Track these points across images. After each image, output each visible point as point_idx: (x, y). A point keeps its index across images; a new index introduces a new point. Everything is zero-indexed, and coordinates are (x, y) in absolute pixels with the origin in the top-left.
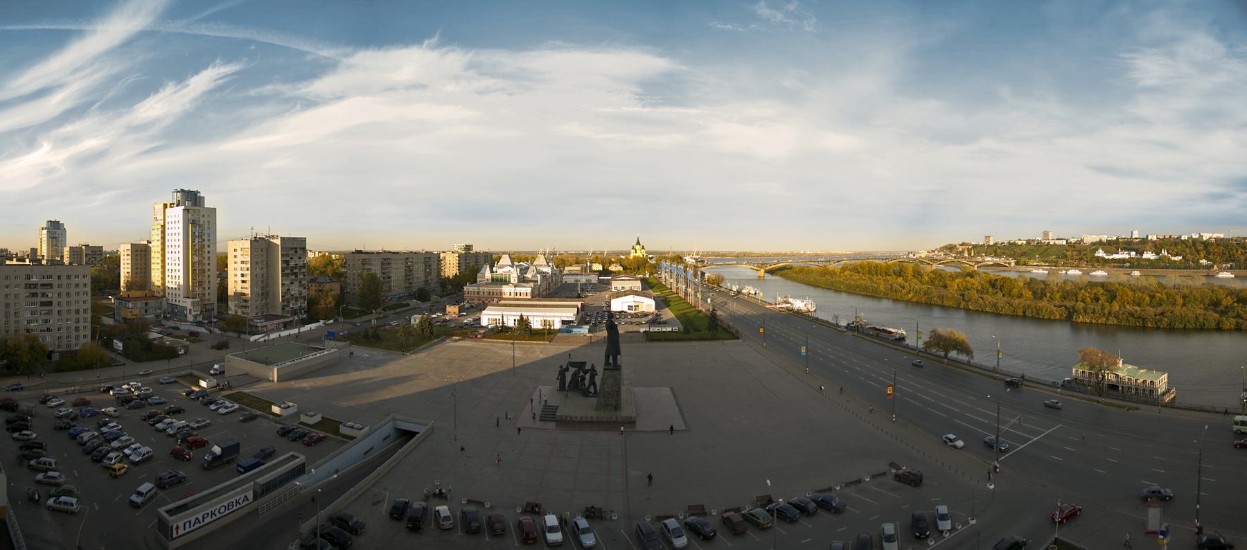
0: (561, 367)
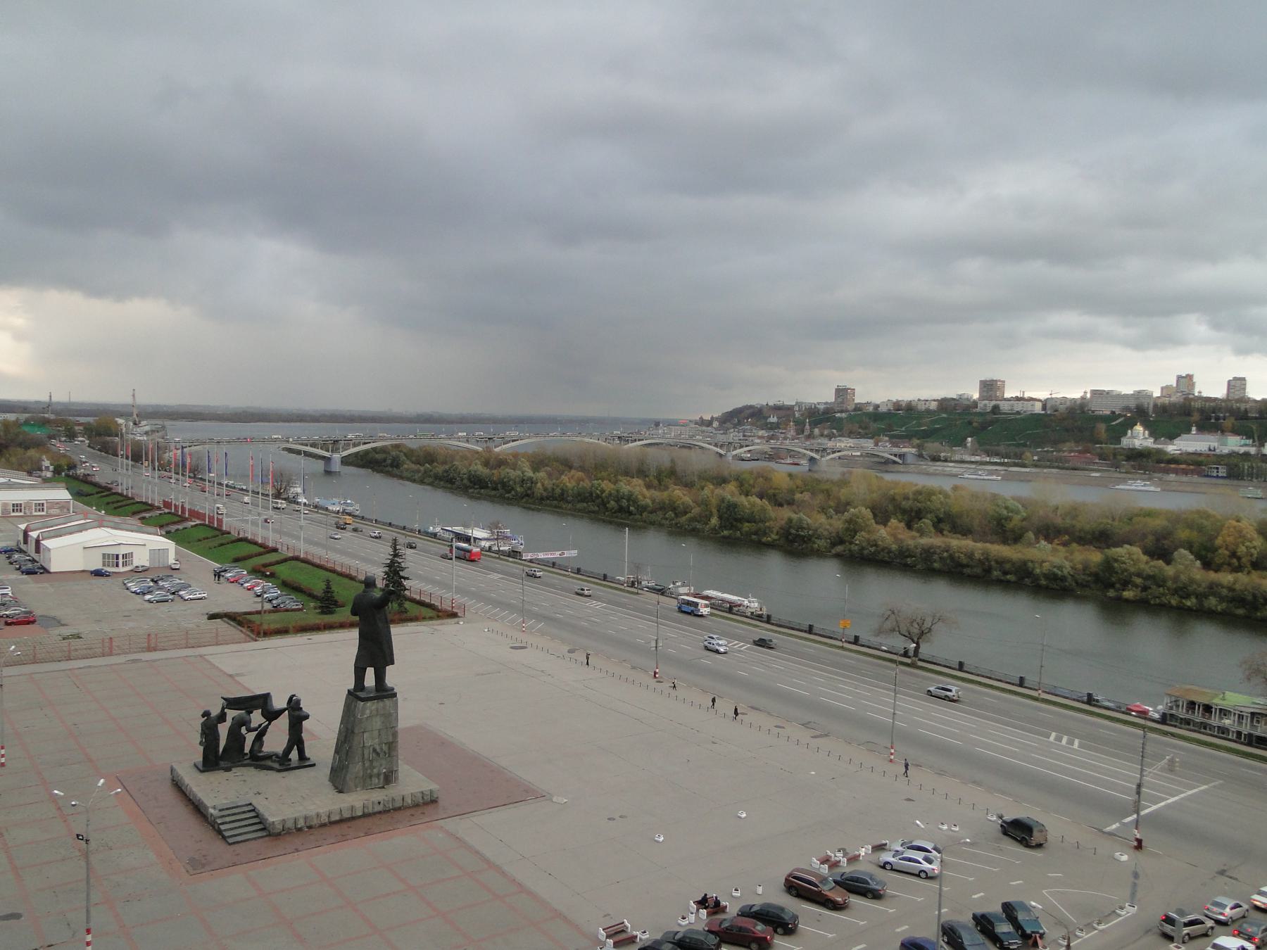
0: (206, 714)
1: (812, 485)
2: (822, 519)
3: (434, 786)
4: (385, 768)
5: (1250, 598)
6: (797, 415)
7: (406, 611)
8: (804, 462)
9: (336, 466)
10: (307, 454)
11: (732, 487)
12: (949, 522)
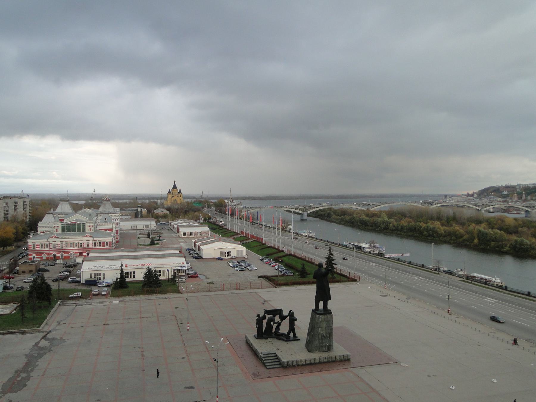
0: (258, 316)
3: (348, 353)
6: (518, 190)
7: (335, 278)
9: (305, 217)
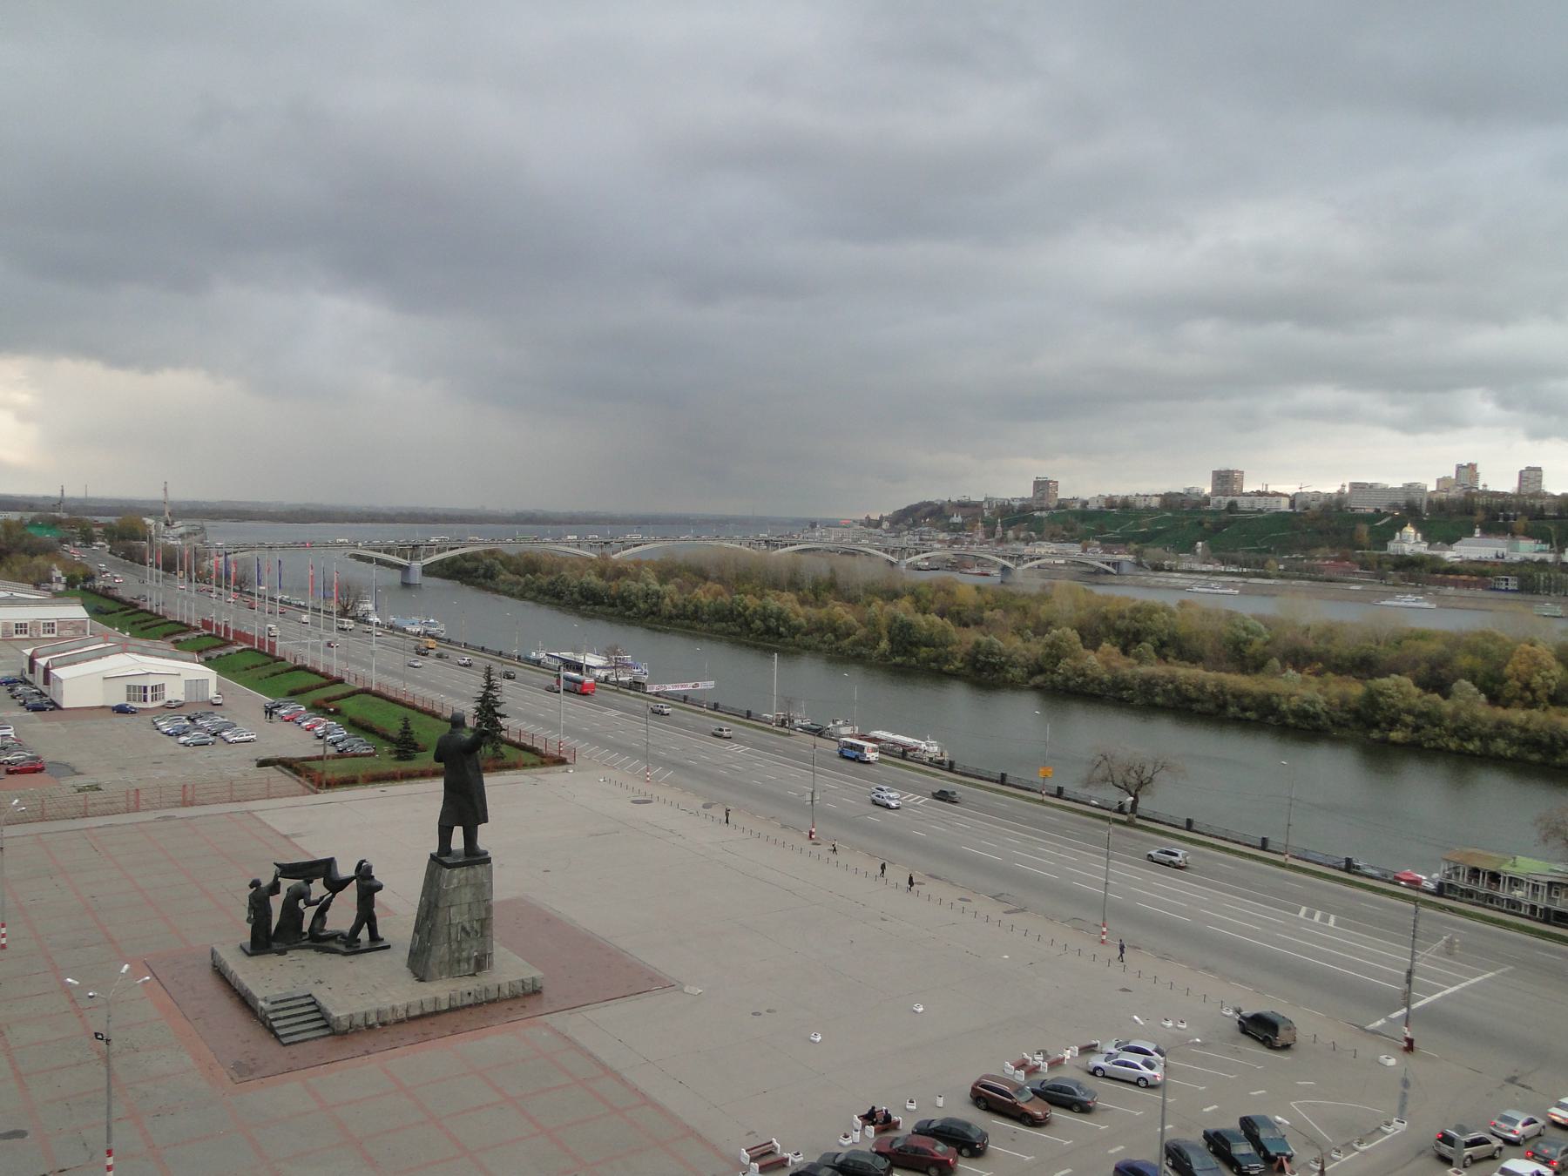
0: (255, 884)
1: (1005, 601)
2: (1017, 642)
3: (537, 974)
4: (476, 951)
5: (1547, 740)
6: (986, 513)
7: (502, 757)
8: (995, 572)
9: (416, 577)
10: (380, 562)
11: (905, 603)
12: (1174, 646)
